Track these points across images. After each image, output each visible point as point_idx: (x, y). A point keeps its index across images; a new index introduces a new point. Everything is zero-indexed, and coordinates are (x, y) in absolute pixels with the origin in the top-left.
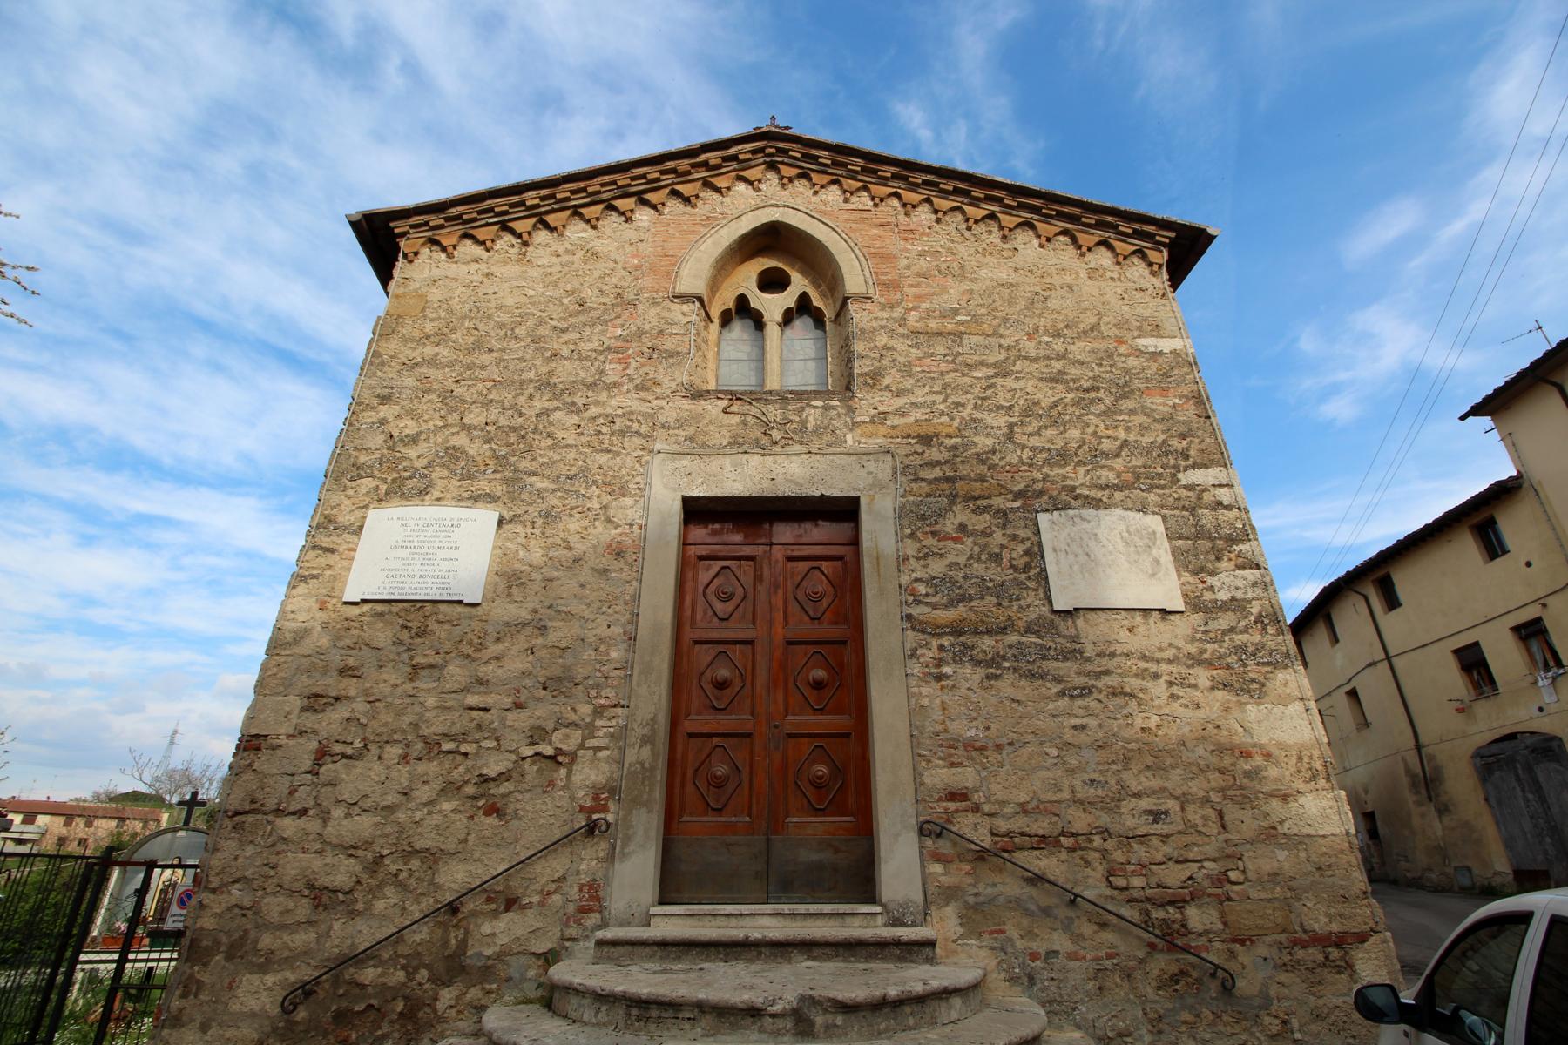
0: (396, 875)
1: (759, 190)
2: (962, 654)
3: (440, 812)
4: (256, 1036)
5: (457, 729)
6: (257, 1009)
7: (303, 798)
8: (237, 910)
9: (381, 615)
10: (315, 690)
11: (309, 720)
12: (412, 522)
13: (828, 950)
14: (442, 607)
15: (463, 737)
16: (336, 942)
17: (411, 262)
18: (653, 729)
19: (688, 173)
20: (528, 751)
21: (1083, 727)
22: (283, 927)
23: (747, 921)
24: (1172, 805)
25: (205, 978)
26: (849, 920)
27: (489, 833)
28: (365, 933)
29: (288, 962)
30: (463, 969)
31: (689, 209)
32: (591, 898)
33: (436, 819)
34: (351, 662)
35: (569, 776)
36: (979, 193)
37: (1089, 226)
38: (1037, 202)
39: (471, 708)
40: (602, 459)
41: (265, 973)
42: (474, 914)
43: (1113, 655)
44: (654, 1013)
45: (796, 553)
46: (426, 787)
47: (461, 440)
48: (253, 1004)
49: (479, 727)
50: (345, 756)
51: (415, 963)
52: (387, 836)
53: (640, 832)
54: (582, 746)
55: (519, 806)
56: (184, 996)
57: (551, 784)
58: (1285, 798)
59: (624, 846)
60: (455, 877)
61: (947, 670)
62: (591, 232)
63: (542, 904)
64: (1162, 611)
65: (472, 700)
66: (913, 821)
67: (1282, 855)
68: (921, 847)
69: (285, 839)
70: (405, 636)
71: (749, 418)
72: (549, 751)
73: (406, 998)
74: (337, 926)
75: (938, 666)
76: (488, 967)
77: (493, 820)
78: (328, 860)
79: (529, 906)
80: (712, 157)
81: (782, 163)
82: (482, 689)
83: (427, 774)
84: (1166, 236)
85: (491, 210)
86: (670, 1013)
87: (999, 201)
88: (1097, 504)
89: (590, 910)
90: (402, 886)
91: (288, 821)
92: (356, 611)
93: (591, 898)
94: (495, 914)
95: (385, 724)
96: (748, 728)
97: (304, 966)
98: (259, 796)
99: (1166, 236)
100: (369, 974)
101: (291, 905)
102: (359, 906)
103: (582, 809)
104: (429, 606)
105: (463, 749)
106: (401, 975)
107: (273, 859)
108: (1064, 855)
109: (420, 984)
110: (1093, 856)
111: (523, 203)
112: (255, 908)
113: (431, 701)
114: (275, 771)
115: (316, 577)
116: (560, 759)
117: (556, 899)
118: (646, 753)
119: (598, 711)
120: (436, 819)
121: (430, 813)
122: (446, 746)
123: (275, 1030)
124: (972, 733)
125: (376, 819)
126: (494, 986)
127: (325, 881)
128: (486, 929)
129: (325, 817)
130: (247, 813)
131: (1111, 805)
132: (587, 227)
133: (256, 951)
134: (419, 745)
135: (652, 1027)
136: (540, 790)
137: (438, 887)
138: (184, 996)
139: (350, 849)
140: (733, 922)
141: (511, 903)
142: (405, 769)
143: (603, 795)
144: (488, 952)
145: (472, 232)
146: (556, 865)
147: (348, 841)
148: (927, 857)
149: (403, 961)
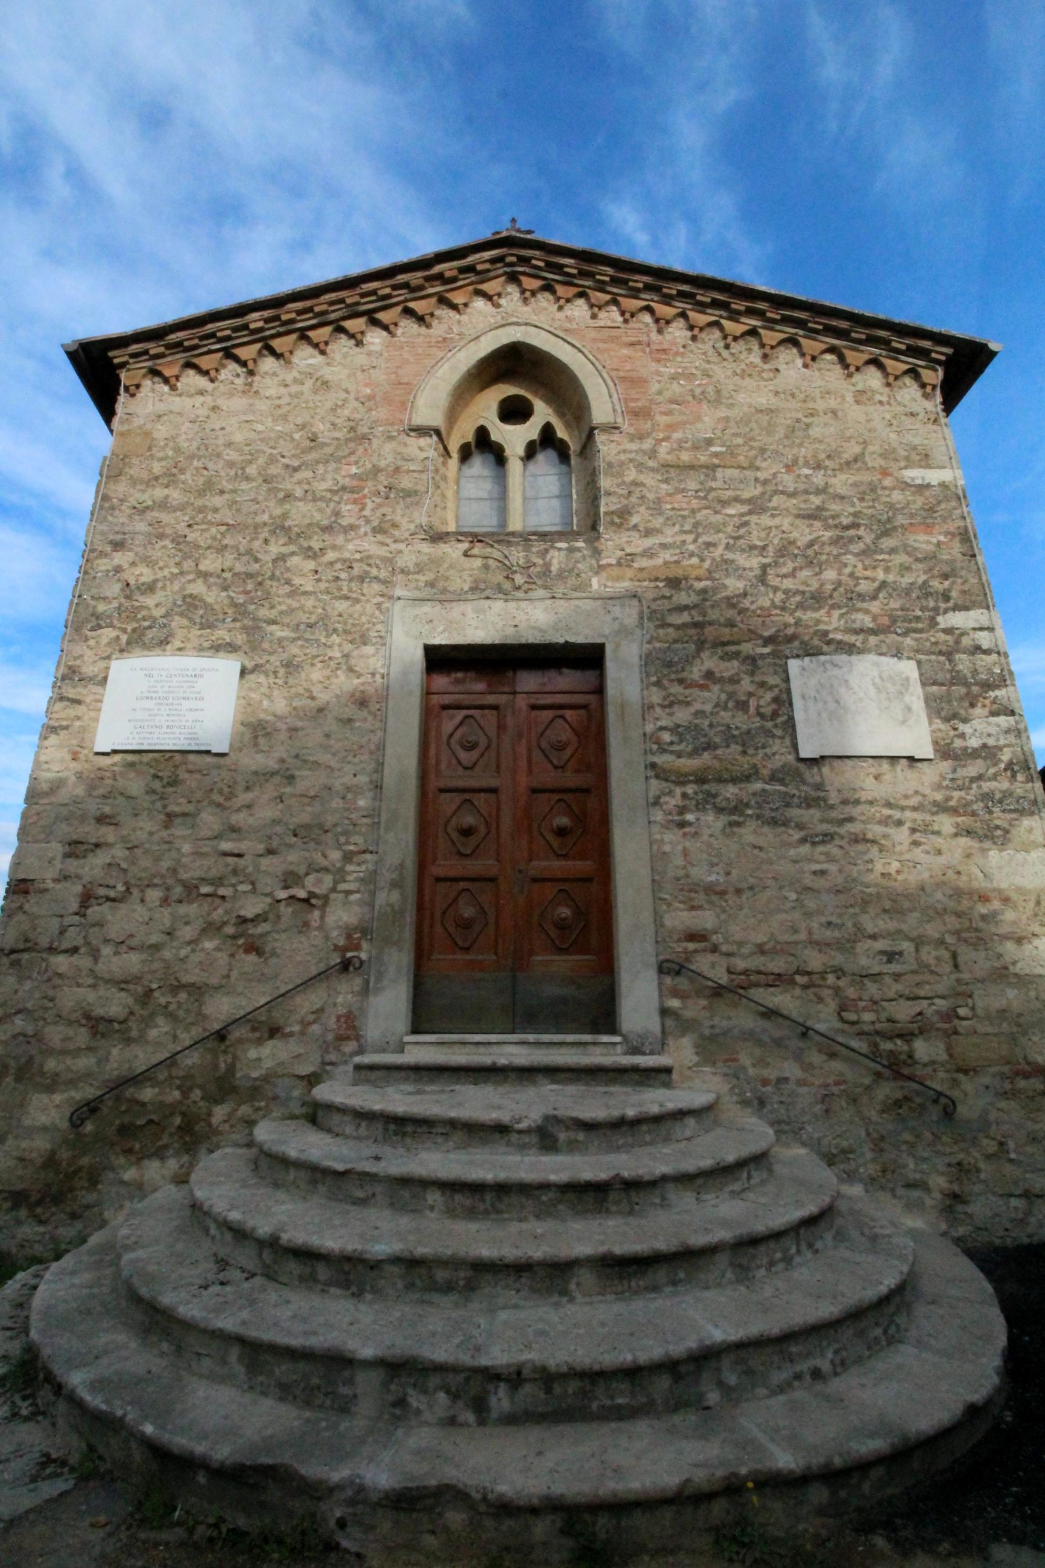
0: (166, 1007)
2: (707, 802)
3: (203, 950)
4: (48, 1146)
5: (214, 873)
6: (48, 1123)
8: (21, 1038)
10: (75, 837)
13: (568, 1075)
16: (115, 1065)
17: (133, 395)
19: (421, 288)
20: (283, 894)
22: (63, 1052)
23: (495, 1049)
24: (906, 946)
26: (591, 1048)
28: (142, 1058)
29: (72, 1083)
30: (233, 1090)
33: (198, 957)
34: (107, 810)
35: (322, 917)
36: (739, 305)
42: (240, 1041)
44: (409, 1129)
46: (188, 928)
47: (198, 588)
48: (43, 1119)
51: (188, 1084)
54: (334, 890)
57: (306, 924)
60: (220, 1009)
61: (690, 817)
62: (319, 359)
63: (302, 1033)
64: (911, 759)
65: (226, 846)
70: (157, 785)
71: (491, 562)
73: (183, 1114)
74: (115, 1052)
77: (252, 958)
79: (291, 1034)
81: (524, 273)
82: (234, 835)
85: (213, 335)
86: (425, 1129)
89: (348, 1038)
90: (172, 1017)
94: (259, 1042)
95: (145, 869)
96: (494, 872)
98: (32, 936)
100: (147, 1094)
101: (71, 1033)
102: (134, 1034)
103: (336, 948)
104: (178, 757)
105: (221, 891)
107: (51, 993)
110: (826, 993)
111: (245, 327)
112: (38, 1036)
113: (186, 848)
115: (66, 728)
116: (313, 901)
119: (348, 857)
120: (198, 957)
121: (193, 951)
122: (205, 889)
125: (144, 956)
126: (263, 1104)
127: (100, 1012)
128: (252, 1054)
131: (847, 945)
132: (315, 352)
133: (42, 1073)
134: (178, 890)
136: (295, 930)
139: (122, 983)
140: (482, 1049)
141: (274, 1032)
142: (166, 911)
144: (255, 1074)
146: (313, 999)
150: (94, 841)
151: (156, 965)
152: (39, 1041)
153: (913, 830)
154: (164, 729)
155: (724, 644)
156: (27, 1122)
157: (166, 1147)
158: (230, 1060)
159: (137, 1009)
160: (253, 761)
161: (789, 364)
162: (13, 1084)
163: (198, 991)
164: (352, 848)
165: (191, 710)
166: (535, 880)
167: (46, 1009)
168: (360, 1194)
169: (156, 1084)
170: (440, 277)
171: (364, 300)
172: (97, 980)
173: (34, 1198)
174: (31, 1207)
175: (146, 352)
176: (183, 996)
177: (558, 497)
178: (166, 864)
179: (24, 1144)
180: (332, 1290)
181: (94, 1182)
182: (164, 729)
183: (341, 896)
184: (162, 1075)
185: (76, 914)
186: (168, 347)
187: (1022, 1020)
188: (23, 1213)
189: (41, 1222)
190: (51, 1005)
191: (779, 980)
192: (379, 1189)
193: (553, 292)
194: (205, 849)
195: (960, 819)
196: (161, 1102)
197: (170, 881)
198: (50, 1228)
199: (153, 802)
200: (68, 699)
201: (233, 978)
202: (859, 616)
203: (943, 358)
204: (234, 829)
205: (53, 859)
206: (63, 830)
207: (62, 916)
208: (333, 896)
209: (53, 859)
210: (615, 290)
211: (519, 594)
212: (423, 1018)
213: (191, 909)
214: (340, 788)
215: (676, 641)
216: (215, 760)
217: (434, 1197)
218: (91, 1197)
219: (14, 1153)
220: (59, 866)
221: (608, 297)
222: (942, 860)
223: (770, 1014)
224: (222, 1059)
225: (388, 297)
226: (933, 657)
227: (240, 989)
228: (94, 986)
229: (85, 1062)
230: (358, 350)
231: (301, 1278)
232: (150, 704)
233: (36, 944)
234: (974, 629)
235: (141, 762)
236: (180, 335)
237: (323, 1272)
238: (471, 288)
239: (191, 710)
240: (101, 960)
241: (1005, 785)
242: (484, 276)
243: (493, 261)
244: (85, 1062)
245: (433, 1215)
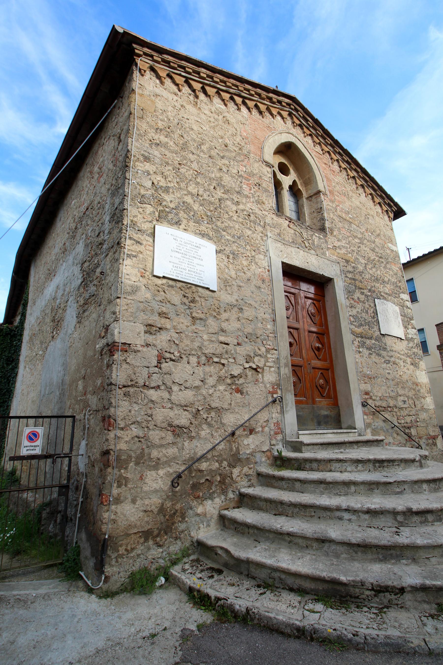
0: (206, 420)
1: (286, 124)
2: (363, 344)
3: (219, 390)
4: (160, 501)
5: (218, 352)
6: (158, 488)
7: (156, 380)
8: (136, 439)
9: (172, 287)
10: (150, 322)
11: (150, 339)
12: (179, 239)
13: (362, 444)
14: (200, 289)
15: (220, 356)
16: (188, 452)
17: (143, 75)
18: (287, 361)
20: (247, 365)
22: (162, 446)
23: (325, 436)
25: (129, 475)
26: (350, 434)
27: (239, 401)
28: (200, 447)
29: (168, 463)
30: (239, 460)
31: (261, 117)
32: (278, 429)
33: (218, 394)
34: (164, 309)
35: (263, 376)
36: (354, 166)
37: (378, 195)
39: (221, 343)
40: (249, 233)
41: (158, 470)
42: (239, 436)
43: (392, 351)
44: (385, 464)
45: (308, 296)
46: (211, 378)
47: (189, 199)
48: (155, 486)
49: (227, 352)
50: (172, 360)
51: (220, 459)
52: (199, 401)
53: (290, 403)
54: (265, 365)
55: (248, 390)
56: (119, 486)
57: (257, 380)
58: (424, 398)
59: (286, 407)
60: (231, 420)
61: (361, 350)
62: (223, 107)
63: (262, 431)
64: (401, 338)
65: (222, 339)
66: (360, 401)
69: (152, 401)
70: (185, 300)
71: (297, 233)
72: (254, 367)
73: (220, 475)
74: (186, 444)
75: (359, 348)
76: (248, 458)
77: (239, 395)
78: (176, 412)
79: (258, 432)
81: (295, 115)
82: (223, 334)
83: (210, 372)
85: (184, 68)
86: (391, 464)
87: (357, 172)
88: (385, 299)
89: (279, 433)
90: (210, 425)
91: (152, 392)
92: (159, 282)
93: (278, 429)
94: (247, 436)
95: (187, 346)
96: (301, 363)
97: (175, 465)
98: (133, 377)
100: (204, 466)
101: (164, 435)
102: (193, 434)
103: (270, 392)
104: (194, 287)
105: (223, 361)
106: (217, 464)
107: (149, 412)
108: (389, 413)
109: (225, 468)
111: (212, 78)
112: (146, 437)
113: (205, 337)
114: (138, 364)
115: (135, 256)
116: (258, 370)
117: (267, 429)
118: (287, 370)
119: (268, 351)
120: (218, 394)
121: (215, 391)
122: (216, 360)
123: (168, 497)
124: (368, 372)
125: (194, 393)
126: (252, 466)
127: (176, 422)
128: (246, 442)
129: (170, 390)
130: (129, 386)
131: (395, 398)
132: (222, 103)
133: (150, 459)
134: (204, 358)
135: (386, 469)
136: (253, 383)
137: (223, 425)
138: (119, 486)
139: (184, 407)
140: (322, 436)
141: (252, 431)
142: (201, 369)
143: (277, 385)
144: (248, 452)
145: (174, 76)
146: (263, 416)
147: (183, 403)
149: (216, 458)
150: (159, 326)
151: (200, 398)
152: (146, 440)
154: (187, 271)
155: (361, 289)
156: (146, 488)
157: (214, 492)
158: (236, 446)
159: (193, 420)
160: (226, 298)
162: (134, 467)
163: (218, 410)
164: (269, 347)
165: (198, 264)
166: (313, 368)
167: (148, 421)
168: (398, 490)
169: (207, 460)
170: (270, 99)
171: (245, 91)
172: (173, 405)
173: (156, 532)
174: (154, 538)
175: (152, 56)
176: (213, 414)
178: (196, 344)
179: (147, 502)
180: (435, 523)
181: (183, 516)
182: (187, 271)
183: (268, 368)
184: (209, 456)
185: (155, 367)
186: (163, 60)
188: (151, 542)
189: (160, 546)
190: (150, 419)
192: (406, 487)
193: (302, 129)
194: (213, 339)
196: (211, 469)
197: (199, 353)
198: (165, 548)
199: (185, 310)
200: (134, 240)
201: (233, 405)
202: (385, 288)
204: (223, 331)
205: (139, 333)
206: (142, 316)
207: (148, 367)
208: (265, 368)
209: (139, 333)
210: (321, 140)
211: (307, 250)
212: (302, 423)
213: (211, 369)
214: (260, 318)
215: (350, 284)
216: (211, 293)
217: (425, 486)
218: (182, 526)
219: (142, 508)
220: (143, 338)
221: (319, 141)
223: (386, 420)
224: (234, 445)
225: (252, 95)
227: (237, 411)
228: (171, 408)
229: (172, 451)
230: (237, 112)
231: (421, 523)
232: (179, 256)
233: (137, 383)
235: (176, 286)
236: (170, 58)
237: (430, 517)
238: (278, 110)
239: (198, 264)
240: (174, 393)
243: (287, 104)
244: (172, 451)
245: (426, 493)
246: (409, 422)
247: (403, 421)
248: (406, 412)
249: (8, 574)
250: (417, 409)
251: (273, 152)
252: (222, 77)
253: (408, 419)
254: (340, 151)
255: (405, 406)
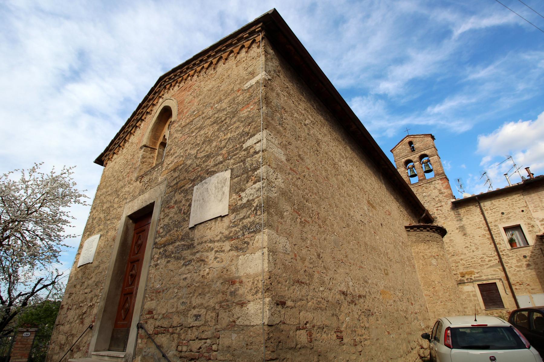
19: (148, 105)
21: (186, 278)
24: (203, 311)
38: (229, 42)
64: (221, 216)
67: (234, 336)
68: (138, 333)
80: (151, 97)
84: (258, 28)
99: (258, 28)
110: (176, 336)
148: (139, 337)
153: (216, 251)
161: (221, 67)
177: (479, 204)
187: (235, 352)
191: (35, 287)
195: (232, 242)
203: (260, 29)
222: (222, 265)
226: (239, 164)
234: (255, 144)
241: (252, 219)
242: (159, 92)
243: (160, 87)
246: (195, 350)
247: (185, 349)
248: (196, 333)
249: (119, 187)
250: (218, 327)
251: (94, 160)
252: (179, 71)
253: (195, 346)
254: (186, 67)
255: (197, 323)
